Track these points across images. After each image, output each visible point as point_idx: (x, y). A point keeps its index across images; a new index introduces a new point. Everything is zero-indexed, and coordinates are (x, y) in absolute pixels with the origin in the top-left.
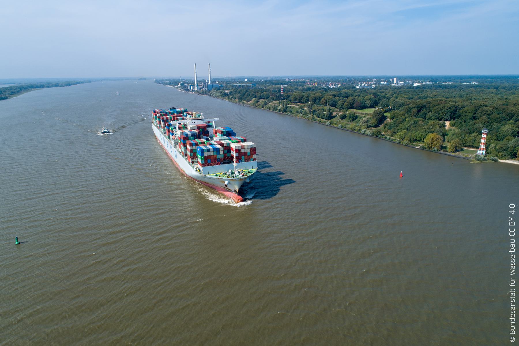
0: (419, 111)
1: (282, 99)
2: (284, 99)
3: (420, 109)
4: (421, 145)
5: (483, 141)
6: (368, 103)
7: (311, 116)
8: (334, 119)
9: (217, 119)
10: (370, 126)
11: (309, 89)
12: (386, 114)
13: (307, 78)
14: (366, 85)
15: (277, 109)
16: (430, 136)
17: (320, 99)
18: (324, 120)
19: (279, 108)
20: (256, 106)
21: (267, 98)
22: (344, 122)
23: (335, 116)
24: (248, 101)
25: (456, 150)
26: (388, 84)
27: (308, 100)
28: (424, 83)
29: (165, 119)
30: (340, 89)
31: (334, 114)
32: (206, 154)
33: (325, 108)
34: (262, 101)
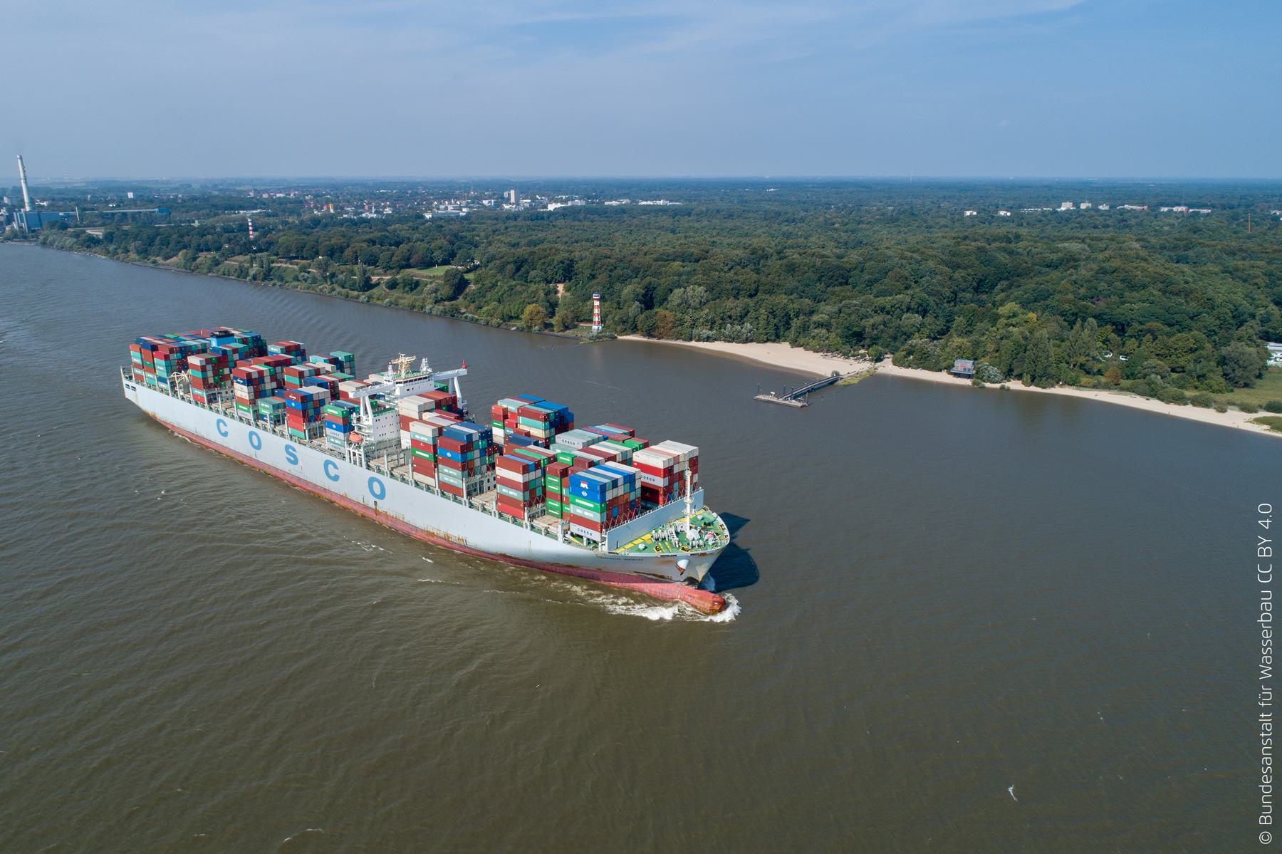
0: (518, 270)
1: (255, 252)
2: (260, 250)
3: (520, 264)
4: (519, 324)
5: (596, 311)
6: (438, 255)
7: (327, 287)
8: (374, 290)
9: (463, 371)
10: (442, 299)
11: (316, 222)
12: (467, 276)
13: (305, 189)
14: (450, 208)
15: (247, 274)
16: (529, 308)
17: (342, 250)
18: (355, 293)
19: (252, 272)
20: (191, 267)
21: (218, 249)
22: (396, 293)
23: (378, 284)
24: (167, 258)
25: (567, 328)
26: (498, 205)
27: (317, 254)
28: (570, 204)
29: (255, 376)
30: (386, 222)
31: (375, 279)
32: (609, 496)
33: (356, 267)
34: (204, 257)
